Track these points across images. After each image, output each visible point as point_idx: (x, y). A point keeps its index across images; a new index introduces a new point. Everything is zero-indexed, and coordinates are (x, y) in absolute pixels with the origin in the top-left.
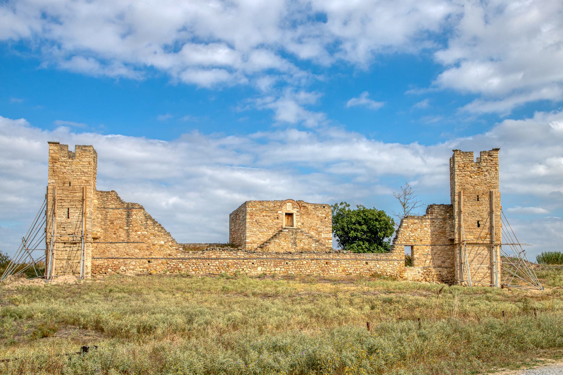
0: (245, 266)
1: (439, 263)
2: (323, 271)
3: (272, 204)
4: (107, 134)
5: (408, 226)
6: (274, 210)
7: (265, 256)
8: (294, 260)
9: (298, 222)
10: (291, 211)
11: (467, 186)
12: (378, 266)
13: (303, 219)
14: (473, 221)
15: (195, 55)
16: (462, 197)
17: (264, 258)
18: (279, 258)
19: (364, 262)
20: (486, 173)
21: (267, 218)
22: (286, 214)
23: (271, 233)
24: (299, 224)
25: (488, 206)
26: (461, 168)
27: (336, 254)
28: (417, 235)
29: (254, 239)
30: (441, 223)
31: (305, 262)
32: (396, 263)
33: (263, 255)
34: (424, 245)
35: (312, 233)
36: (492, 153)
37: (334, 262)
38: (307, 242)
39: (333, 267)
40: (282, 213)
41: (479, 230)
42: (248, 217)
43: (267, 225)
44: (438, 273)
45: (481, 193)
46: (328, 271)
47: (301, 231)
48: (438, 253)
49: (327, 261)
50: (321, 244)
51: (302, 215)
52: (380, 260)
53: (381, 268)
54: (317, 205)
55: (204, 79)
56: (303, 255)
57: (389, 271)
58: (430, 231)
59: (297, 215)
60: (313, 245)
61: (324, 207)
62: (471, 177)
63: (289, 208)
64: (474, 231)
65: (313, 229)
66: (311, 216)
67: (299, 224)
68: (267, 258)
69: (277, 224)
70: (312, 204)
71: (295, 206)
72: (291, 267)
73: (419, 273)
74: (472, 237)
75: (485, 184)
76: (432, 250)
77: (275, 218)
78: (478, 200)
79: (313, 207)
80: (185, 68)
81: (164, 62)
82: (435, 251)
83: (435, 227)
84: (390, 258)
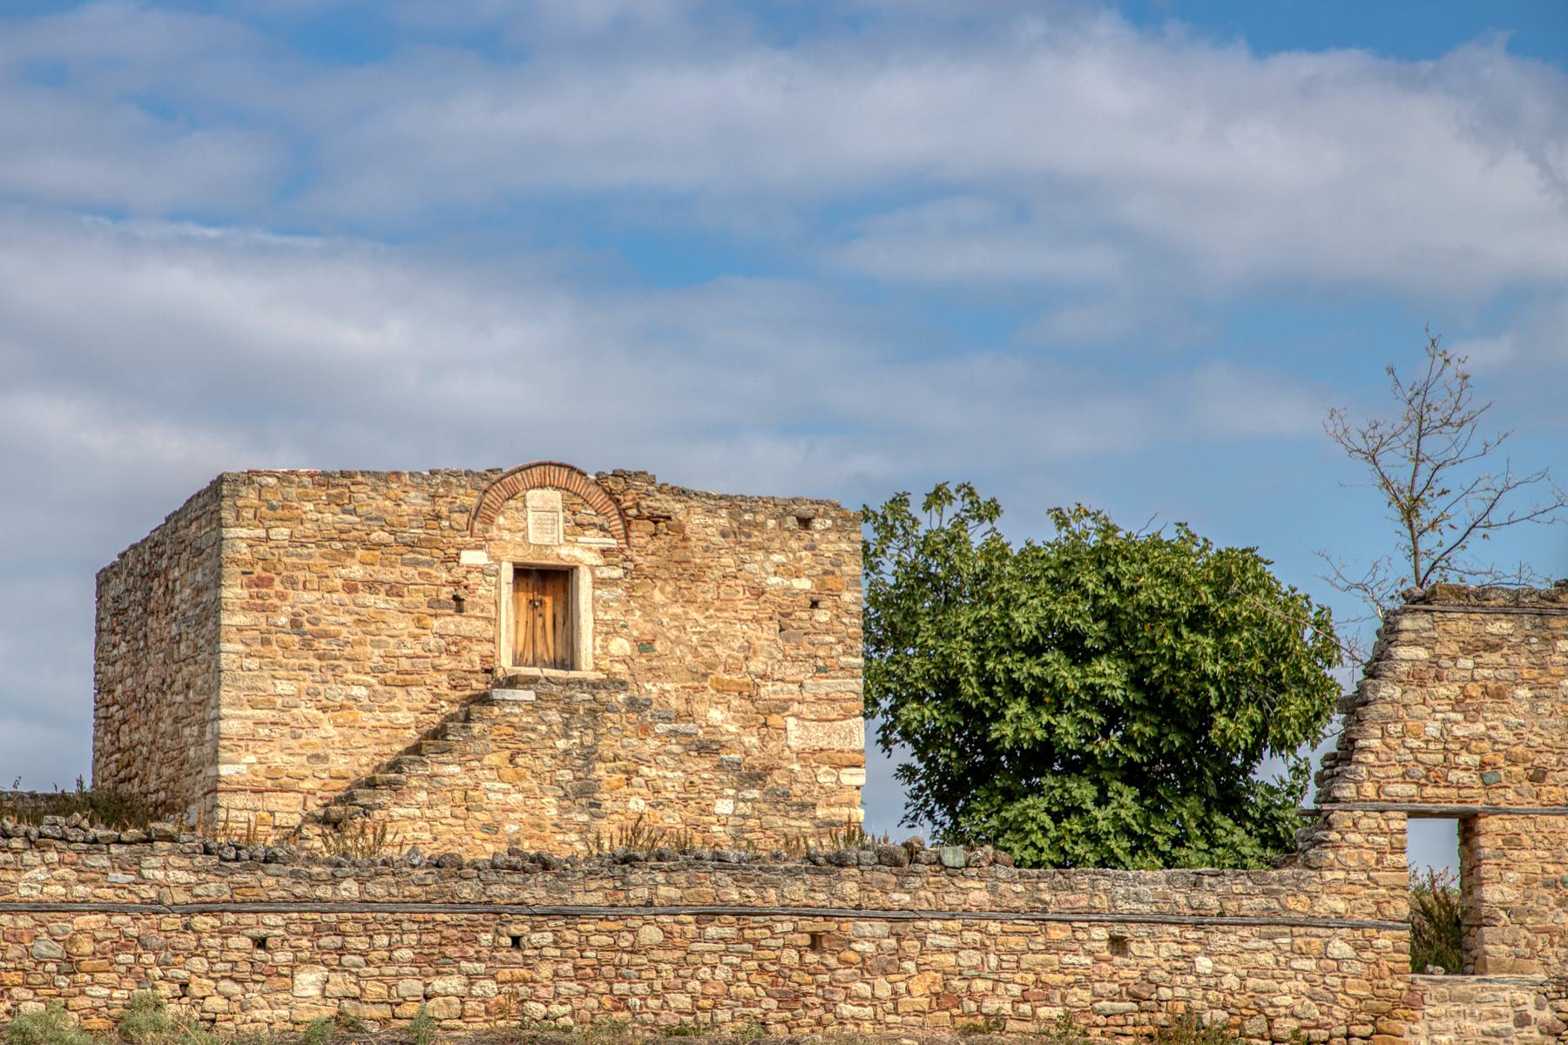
0: (199, 964)
3: (416, 500)
5: (1434, 662)
6: (430, 543)
7: (349, 889)
8: (570, 915)
9: (608, 631)
10: (565, 554)
12: (1204, 964)
13: (649, 609)
17: (341, 905)
19: (1100, 933)
21: (378, 601)
22: (523, 573)
23: (407, 715)
24: (620, 646)
27: (885, 875)
28: (1504, 734)
29: (278, 759)
32: (1339, 948)
33: (335, 881)
35: (716, 715)
37: (869, 937)
39: (865, 968)
40: (487, 563)
42: (233, 591)
46: (828, 1004)
47: (632, 703)
49: (820, 925)
50: (780, 798)
52: (1223, 920)
54: (753, 504)
56: (636, 876)
59: (599, 583)
60: (724, 807)
61: (805, 522)
63: (541, 525)
67: (620, 646)
68: (366, 903)
69: (455, 645)
71: (587, 515)
72: (546, 971)
73: (1522, 1021)
77: (435, 603)
79: (723, 521)
84: (1298, 905)
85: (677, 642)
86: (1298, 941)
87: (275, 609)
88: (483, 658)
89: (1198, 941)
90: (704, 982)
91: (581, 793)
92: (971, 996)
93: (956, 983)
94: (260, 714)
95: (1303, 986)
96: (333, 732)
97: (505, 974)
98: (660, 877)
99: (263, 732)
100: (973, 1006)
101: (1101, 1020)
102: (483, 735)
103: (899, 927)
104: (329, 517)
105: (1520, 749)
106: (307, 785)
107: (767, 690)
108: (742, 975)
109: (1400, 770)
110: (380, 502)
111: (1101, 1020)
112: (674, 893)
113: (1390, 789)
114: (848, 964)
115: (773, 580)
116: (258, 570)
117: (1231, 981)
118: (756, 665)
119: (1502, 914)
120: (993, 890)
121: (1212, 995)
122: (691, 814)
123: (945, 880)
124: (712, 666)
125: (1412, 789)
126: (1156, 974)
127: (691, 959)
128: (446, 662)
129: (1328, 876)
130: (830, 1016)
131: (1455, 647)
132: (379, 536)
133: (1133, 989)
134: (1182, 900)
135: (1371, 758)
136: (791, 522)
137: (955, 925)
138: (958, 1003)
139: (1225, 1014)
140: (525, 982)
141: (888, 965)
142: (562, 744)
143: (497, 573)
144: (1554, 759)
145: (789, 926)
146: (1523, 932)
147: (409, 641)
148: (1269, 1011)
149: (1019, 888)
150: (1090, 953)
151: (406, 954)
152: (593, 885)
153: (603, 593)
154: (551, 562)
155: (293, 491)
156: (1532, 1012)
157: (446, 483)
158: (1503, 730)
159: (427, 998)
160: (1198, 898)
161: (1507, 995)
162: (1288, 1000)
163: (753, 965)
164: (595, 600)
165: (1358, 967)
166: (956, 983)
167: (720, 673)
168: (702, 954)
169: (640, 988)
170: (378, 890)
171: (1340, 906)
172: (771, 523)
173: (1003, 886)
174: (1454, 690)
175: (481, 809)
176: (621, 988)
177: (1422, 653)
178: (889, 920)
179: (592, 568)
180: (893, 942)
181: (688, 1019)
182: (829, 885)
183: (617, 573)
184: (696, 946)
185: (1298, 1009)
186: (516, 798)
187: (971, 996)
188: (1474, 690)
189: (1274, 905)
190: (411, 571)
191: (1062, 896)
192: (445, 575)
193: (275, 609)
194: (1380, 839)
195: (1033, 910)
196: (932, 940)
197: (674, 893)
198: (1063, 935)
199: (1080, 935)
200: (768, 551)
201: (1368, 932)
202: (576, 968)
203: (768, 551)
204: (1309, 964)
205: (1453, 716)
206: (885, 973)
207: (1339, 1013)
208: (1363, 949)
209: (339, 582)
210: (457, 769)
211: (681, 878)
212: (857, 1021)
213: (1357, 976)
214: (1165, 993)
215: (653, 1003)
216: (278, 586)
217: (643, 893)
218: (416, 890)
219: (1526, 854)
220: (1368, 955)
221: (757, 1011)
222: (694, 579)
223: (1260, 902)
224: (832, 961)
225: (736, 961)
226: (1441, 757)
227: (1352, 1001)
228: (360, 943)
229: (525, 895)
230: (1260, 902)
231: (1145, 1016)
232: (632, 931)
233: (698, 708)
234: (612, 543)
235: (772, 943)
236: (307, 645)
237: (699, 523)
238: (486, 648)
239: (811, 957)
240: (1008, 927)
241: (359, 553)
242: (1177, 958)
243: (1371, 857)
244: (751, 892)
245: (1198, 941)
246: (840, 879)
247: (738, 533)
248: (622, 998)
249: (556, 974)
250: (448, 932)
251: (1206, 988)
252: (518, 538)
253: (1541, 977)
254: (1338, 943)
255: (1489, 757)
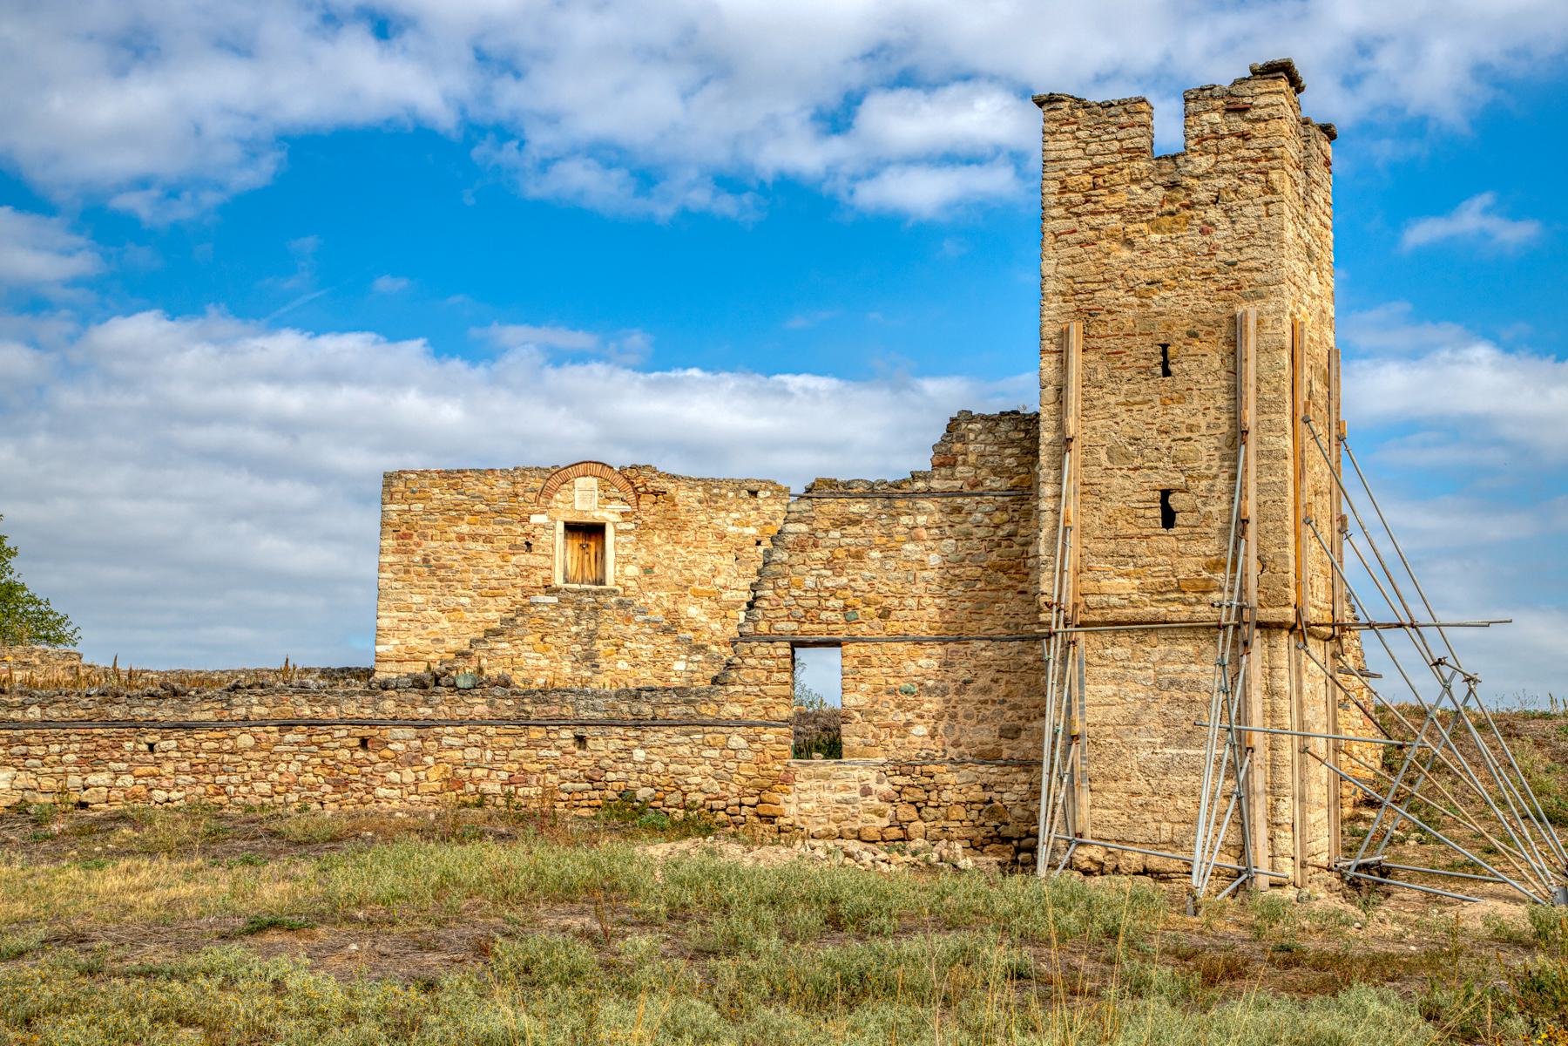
1: (985, 736)
2: (341, 785)
3: (503, 485)
4: (652, 371)
5: (812, 534)
6: (511, 511)
7: (34, 713)
8: (189, 727)
9: (625, 561)
10: (596, 515)
11: (1106, 295)
12: (639, 754)
13: (650, 548)
14: (1133, 490)
15: (902, 122)
16: (1076, 358)
17: (31, 724)
18: (107, 724)
19: (567, 733)
20: (1213, 214)
21: (477, 546)
22: (572, 529)
24: (632, 570)
25: (1222, 401)
26: (1077, 198)
27: (415, 695)
28: (861, 584)
29: (413, 642)
30: (999, 517)
31: (246, 740)
33: (24, 707)
34: (903, 638)
35: (693, 611)
36: (1246, 95)
37: (401, 740)
38: (646, 651)
39: (397, 762)
40: (548, 523)
41: (1167, 541)
43: (475, 579)
44: (976, 793)
45: (1179, 332)
46: (370, 789)
47: (620, 603)
48: (981, 682)
49: (366, 731)
51: (643, 529)
52: (654, 723)
53: (658, 767)
54: (719, 483)
55: (921, 192)
56: (237, 700)
57: (700, 780)
58: (934, 559)
59: (619, 532)
60: (679, 666)
61: (754, 493)
62: (1129, 243)
63: (584, 499)
64: (1142, 548)
65: (697, 594)
66: (687, 536)
67: (632, 570)
68: (47, 723)
69: (526, 571)
70: (693, 483)
71: (613, 492)
72: (169, 768)
73: (866, 792)
74: (1127, 585)
75: (1207, 276)
76: (946, 665)
77: (513, 546)
78: (1167, 373)
79: (700, 493)
80: (875, 168)
81: (804, 155)
82: (962, 674)
83: (968, 536)
85: (669, 567)
86: (708, 737)
87: (413, 552)
88: (544, 579)
89: (637, 738)
90: (281, 774)
91: (586, 659)
92: (471, 780)
93: (461, 771)
94: (403, 615)
95: (709, 769)
96: (447, 624)
97: (141, 770)
98: (255, 700)
99: (404, 625)
100: (472, 788)
101: (564, 796)
102: (523, 625)
103: (422, 732)
104: (448, 497)
105: (872, 595)
106: (431, 657)
107: (727, 595)
108: (309, 768)
109: (785, 612)
110: (481, 487)
111: (564, 796)
112: (263, 710)
113: (778, 626)
114: (385, 759)
115: (731, 529)
116: (403, 529)
117: (658, 767)
118: (720, 581)
119: (857, 715)
120: (491, 704)
121: (643, 777)
122: (658, 670)
123: (457, 698)
124: (691, 582)
125: (794, 626)
126: (606, 763)
127: (273, 757)
128: (519, 581)
129: (731, 689)
130: (370, 797)
131: (827, 523)
132: (480, 507)
133: (588, 773)
134: (625, 708)
135: (765, 604)
136: (744, 493)
137: (463, 730)
138: (462, 785)
139: (652, 791)
140: (154, 776)
141: (414, 759)
142: (574, 629)
143: (554, 528)
144: (896, 602)
145: (344, 733)
146: (871, 727)
147: (496, 570)
148: (684, 788)
149: (510, 702)
150: (558, 748)
151: (71, 757)
152: (206, 706)
153: (622, 539)
154: (589, 520)
155: (427, 482)
156: (873, 785)
157: (523, 475)
158: (861, 582)
159: (85, 789)
160: (636, 707)
161: (856, 774)
162: (698, 780)
163: (318, 760)
164: (616, 543)
165: (749, 755)
166: (461, 771)
167: (696, 585)
168: (281, 754)
169: (234, 779)
170: (54, 713)
171: (739, 711)
172: (731, 494)
173: (498, 701)
174: (826, 554)
175: (521, 669)
176: (221, 779)
177: (803, 528)
178: (417, 727)
179: (615, 524)
180: (418, 742)
181: (266, 800)
182: (375, 703)
183: (632, 526)
184: (277, 748)
185: (704, 786)
186: (544, 663)
187: (471, 780)
188: (840, 553)
189: (692, 711)
190: (499, 528)
191: (540, 708)
192: (520, 530)
193: (413, 552)
194: (769, 662)
195: (519, 718)
196: (446, 741)
197: (263, 710)
198: (540, 736)
199: (552, 735)
200: (728, 511)
201: (758, 729)
202: (192, 765)
203: (728, 511)
204: (715, 753)
205: (824, 572)
206: (411, 765)
207: (734, 788)
208: (753, 741)
209: (453, 536)
210: (506, 645)
211: (269, 700)
212: (388, 799)
213: (748, 762)
214: (610, 776)
215: (243, 789)
216: (415, 539)
217: (243, 711)
218: (81, 712)
219: (875, 671)
220: (757, 746)
221: (316, 794)
222: (680, 529)
223: (681, 709)
224: (373, 757)
225: (304, 758)
226: (815, 602)
227: (743, 780)
228: (40, 751)
229: (158, 714)
230: (681, 709)
231: (597, 793)
232: (233, 738)
233: (681, 607)
234: (628, 508)
235: (332, 745)
236: (433, 573)
237: (684, 496)
238: (546, 573)
239: (360, 754)
240: (501, 730)
241: (467, 517)
242: (621, 751)
243: (762, 675)
244: (319, 709)
245: (637, 738)
246: (383, 699)
247: (710, 501)
248: (223, 786)
249: (177, 770)
250: (101, 742)
251: (641, 772)
252: (568, 506)
253: (882, 760)
254: (735, 737)
255: (851, 601)
